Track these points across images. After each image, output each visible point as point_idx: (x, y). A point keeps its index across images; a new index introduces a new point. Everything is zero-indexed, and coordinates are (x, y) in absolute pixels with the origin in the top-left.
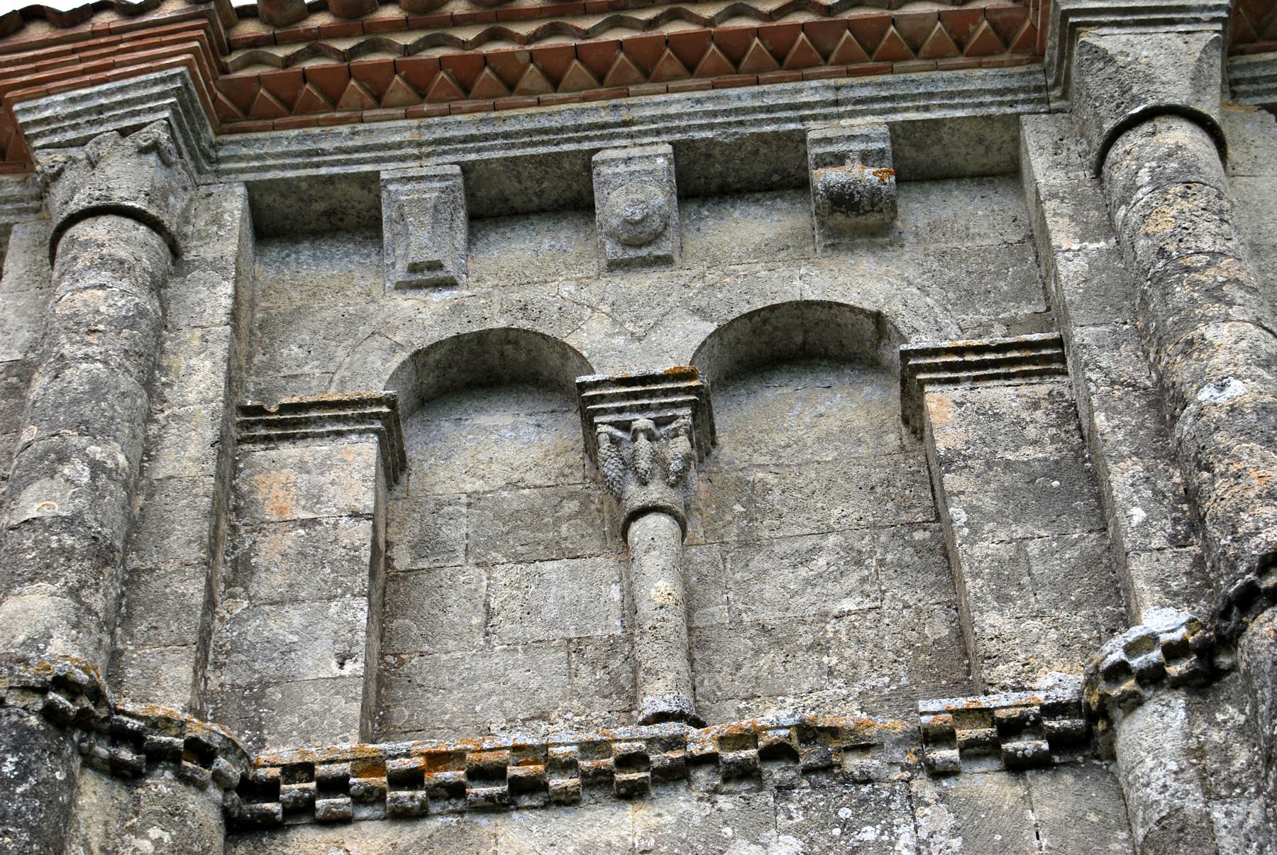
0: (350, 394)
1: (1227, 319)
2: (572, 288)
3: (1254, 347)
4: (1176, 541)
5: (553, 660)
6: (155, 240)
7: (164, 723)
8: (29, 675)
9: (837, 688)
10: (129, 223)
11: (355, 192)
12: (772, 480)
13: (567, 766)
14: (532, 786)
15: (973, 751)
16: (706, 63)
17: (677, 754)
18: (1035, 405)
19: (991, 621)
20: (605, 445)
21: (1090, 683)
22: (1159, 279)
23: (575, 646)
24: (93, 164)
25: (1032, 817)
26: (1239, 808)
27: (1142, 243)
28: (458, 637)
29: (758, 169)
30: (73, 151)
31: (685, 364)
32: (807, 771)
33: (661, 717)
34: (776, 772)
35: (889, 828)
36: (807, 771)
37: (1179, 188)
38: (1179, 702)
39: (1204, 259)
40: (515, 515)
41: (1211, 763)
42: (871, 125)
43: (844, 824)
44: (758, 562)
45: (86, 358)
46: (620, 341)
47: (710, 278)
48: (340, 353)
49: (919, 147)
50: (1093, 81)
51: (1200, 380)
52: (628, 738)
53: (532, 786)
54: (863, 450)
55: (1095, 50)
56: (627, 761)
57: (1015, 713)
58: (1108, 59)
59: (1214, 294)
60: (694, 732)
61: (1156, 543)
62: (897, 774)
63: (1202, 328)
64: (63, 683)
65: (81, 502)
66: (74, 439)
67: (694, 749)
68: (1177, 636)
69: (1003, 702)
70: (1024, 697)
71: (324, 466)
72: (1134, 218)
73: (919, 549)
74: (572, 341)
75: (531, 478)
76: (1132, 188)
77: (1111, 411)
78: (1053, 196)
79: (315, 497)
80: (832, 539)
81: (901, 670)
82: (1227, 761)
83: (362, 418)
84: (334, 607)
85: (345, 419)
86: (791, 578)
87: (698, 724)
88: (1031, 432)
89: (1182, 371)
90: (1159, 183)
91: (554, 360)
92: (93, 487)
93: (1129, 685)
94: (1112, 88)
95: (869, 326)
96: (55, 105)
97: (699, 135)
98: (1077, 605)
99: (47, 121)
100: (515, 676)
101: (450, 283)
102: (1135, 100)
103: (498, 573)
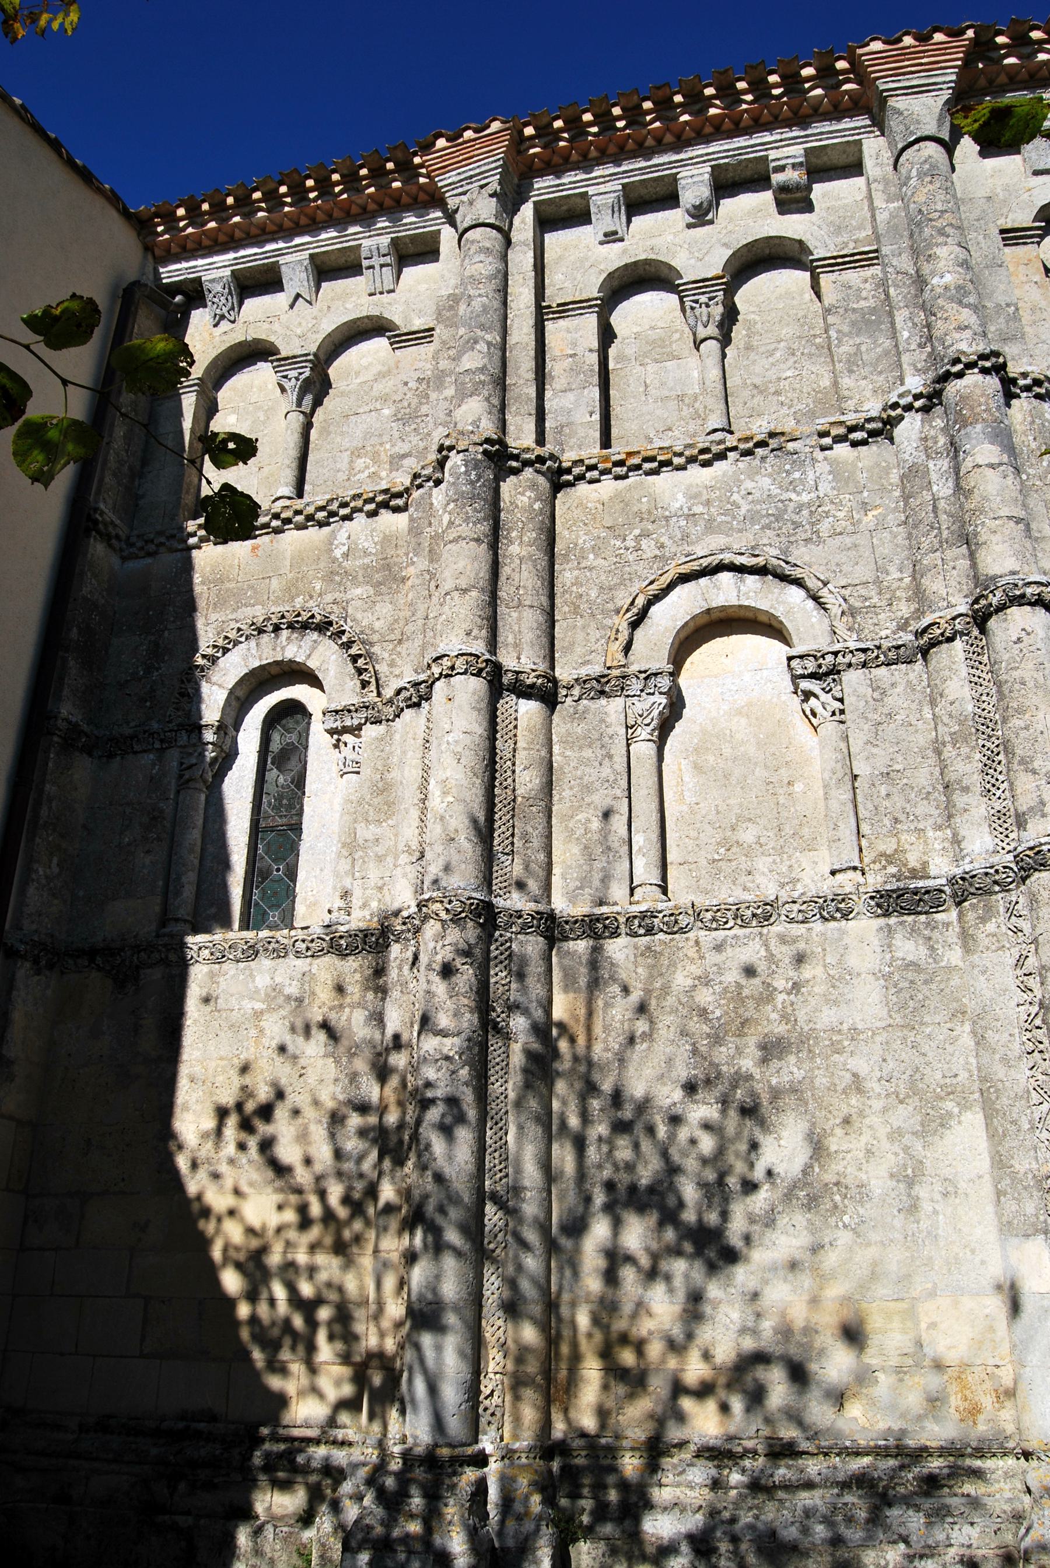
0: (584, 297)
1: (946, 244)
2: (671, 237)
3: (957, 257)
4: (921, 346)
5: (673, 404)
6: (499, 236)
7: (527, 450)
8: (476, 439)
9: (785, 410)
10: (488, 229)
11: (578, 200)
12: (757, 318)
13: (680, 455)
14: (668, 463)
15: (839, 439)
16: (725, 127)
17: (722, 447)
18: (866, 281)
19: (846, 382)
20: (688, 310)
21: (884, 410)
22: (918, 224)
23: (680, 398)
24: (471, 203)
25: (860, 465)
26: (939, 463)
27: (912, 206)
28: (634, 397)
29: (748, 173)
30: (463, 198)
31: (720, 272)
32: (773, 450)
33: (715, 431)
34: (760, 452)
35: (804, 473)
36: (773, 450)
37: (929, 179)
38: (919, 416)
39: (937, 214)
40: (654, 341)
41: (930, 444)
42: (796, 152)
43: (787, 472)
44: (753, 356)
45: (480, 295)
46: (692, 261)
47: (729, 228)
48: (579, 276)
49: (817, 157)
50: (893, 123)
51: (933, 273)
52: (703, 442)
53: (668, 463)
54: (795, 302)
55: (894, 109)
56: (703, 451)
57: (854, 423)
58: (900, 113)
59: (941, 232)
60: (729, 436)
61: (913, 347)
62: (807, 449)
63: (935, 249)
64: (487, 441)
65: (485, 360)
66: (479, 333)
67: (728, 444)
68: (918, 391)
69: (851, 418)
70: (859, 415)
71: (577, 330)
72: (909, 193)
73: (819, 347)
74: (673, 263)
75: (660, 324)
76: (909, 178)
77: (897, 286)
78: (875, 181)
79: (574, 344)
80: (782, 344)
81: (810, 401)
82: (936, 443)
83: (590, 307)
84: (586, 391)
85: (583, 308)
86: (765, 362)
87: (731, 433)
88: (864, 294)
89: (926, 269)
90: (921, 175)
91: (666, 271)
92: (489, 353)
93: (899, 411)
94: (902, 127)
95: (797, 245)
96: (452, 177)
97: (722, 161)
98: (881, 373)
99: (450, 184)
100: (658, 412)
101: (622, 240)
102: (912, 133)
103: (649, 368)
